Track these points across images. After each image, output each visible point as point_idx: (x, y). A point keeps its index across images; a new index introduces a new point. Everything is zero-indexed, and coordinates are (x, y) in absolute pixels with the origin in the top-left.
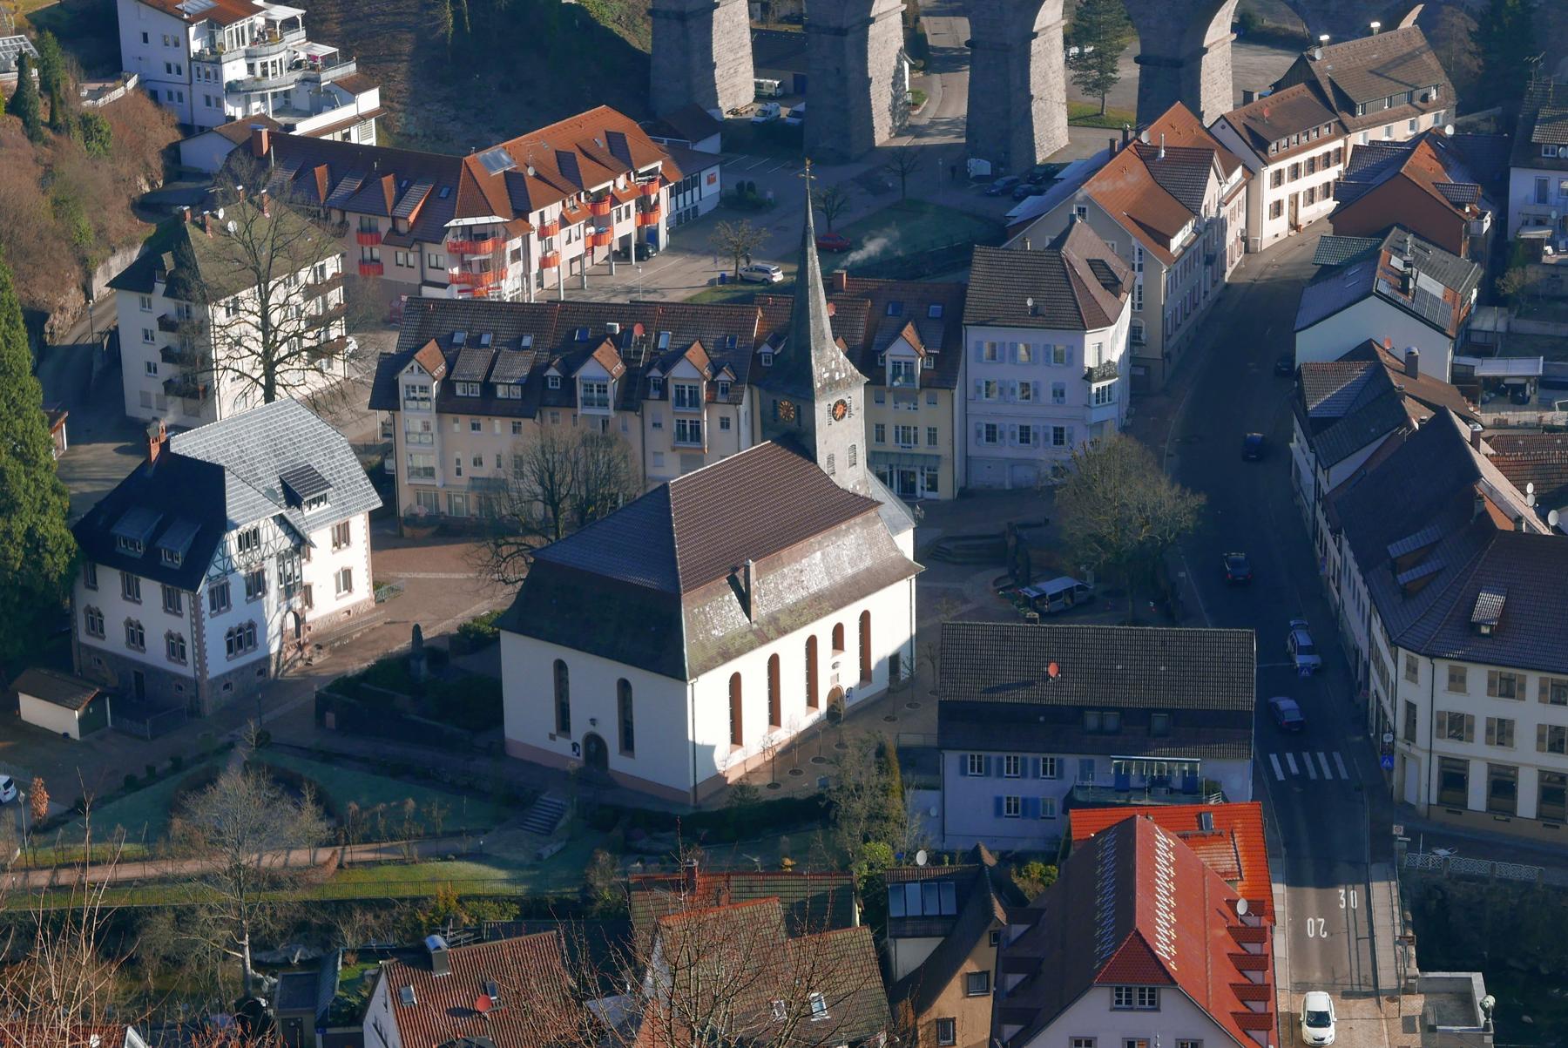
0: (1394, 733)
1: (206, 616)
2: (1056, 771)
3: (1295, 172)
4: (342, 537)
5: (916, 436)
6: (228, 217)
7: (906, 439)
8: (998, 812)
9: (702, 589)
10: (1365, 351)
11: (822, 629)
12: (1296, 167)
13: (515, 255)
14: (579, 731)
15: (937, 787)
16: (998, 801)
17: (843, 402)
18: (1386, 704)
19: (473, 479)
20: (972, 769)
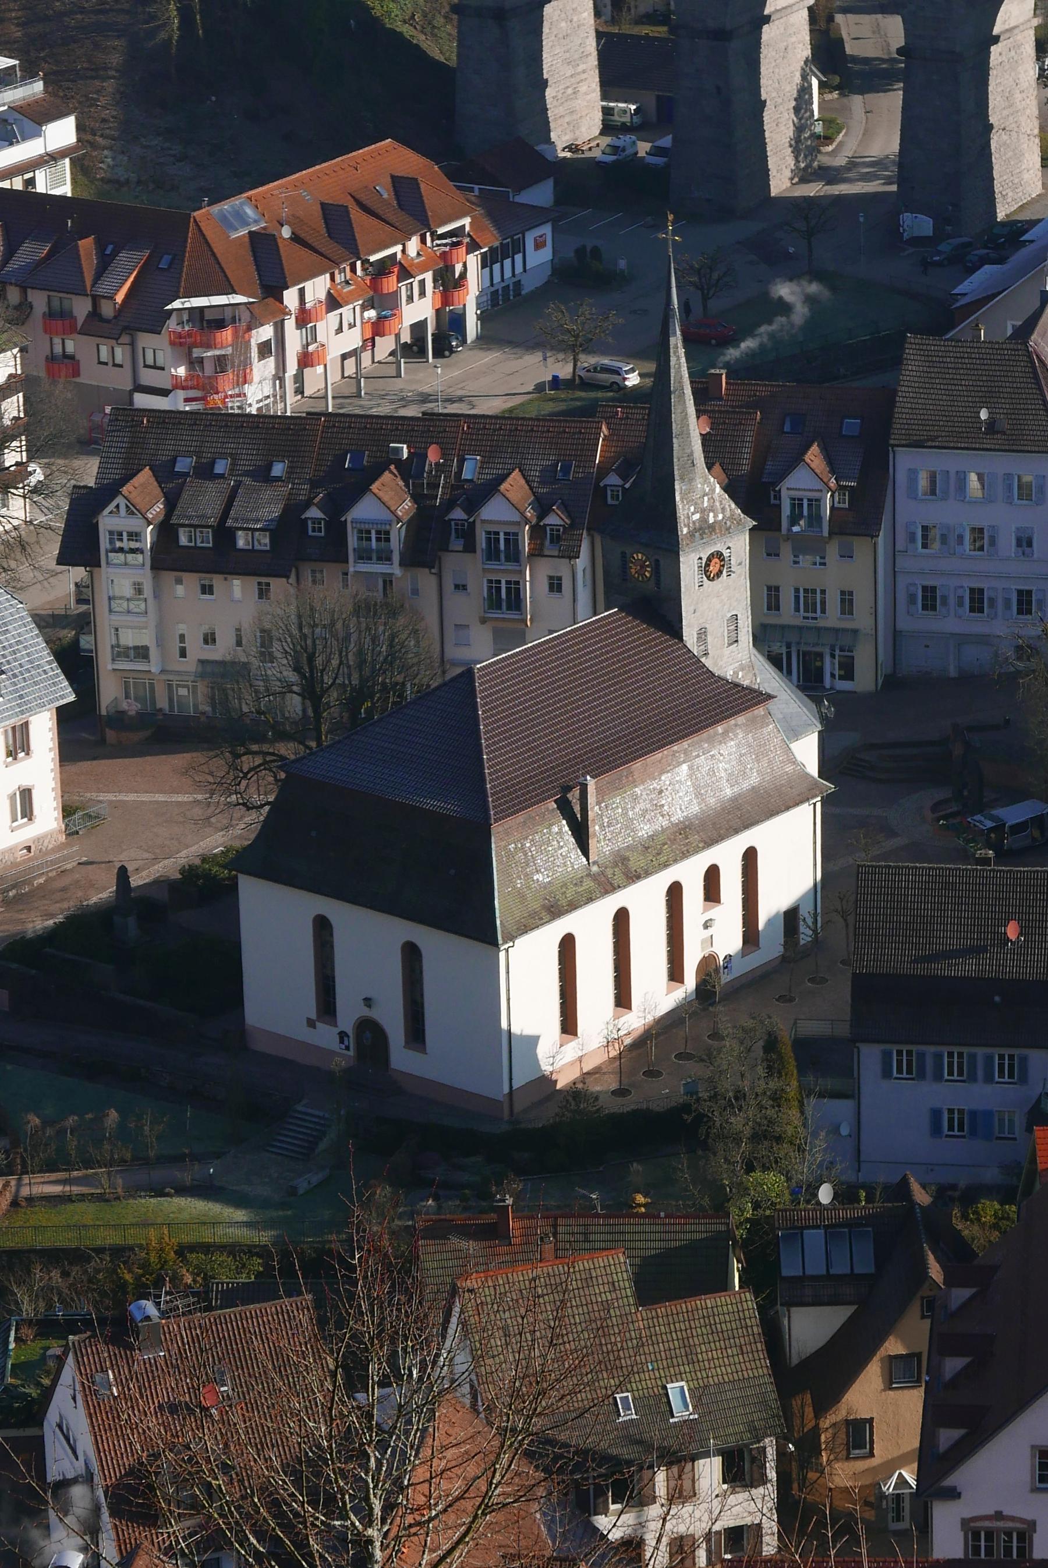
5: (823, 603)
7: (810, 607)
8: (936, 1130)
9: (521, 817)
13: (265, 349)
14: (349, 1012)
15: (851, 1093)
16: (936, 1114)
17: (719, 555)
19: (202, 662)
20: (900, 1070)
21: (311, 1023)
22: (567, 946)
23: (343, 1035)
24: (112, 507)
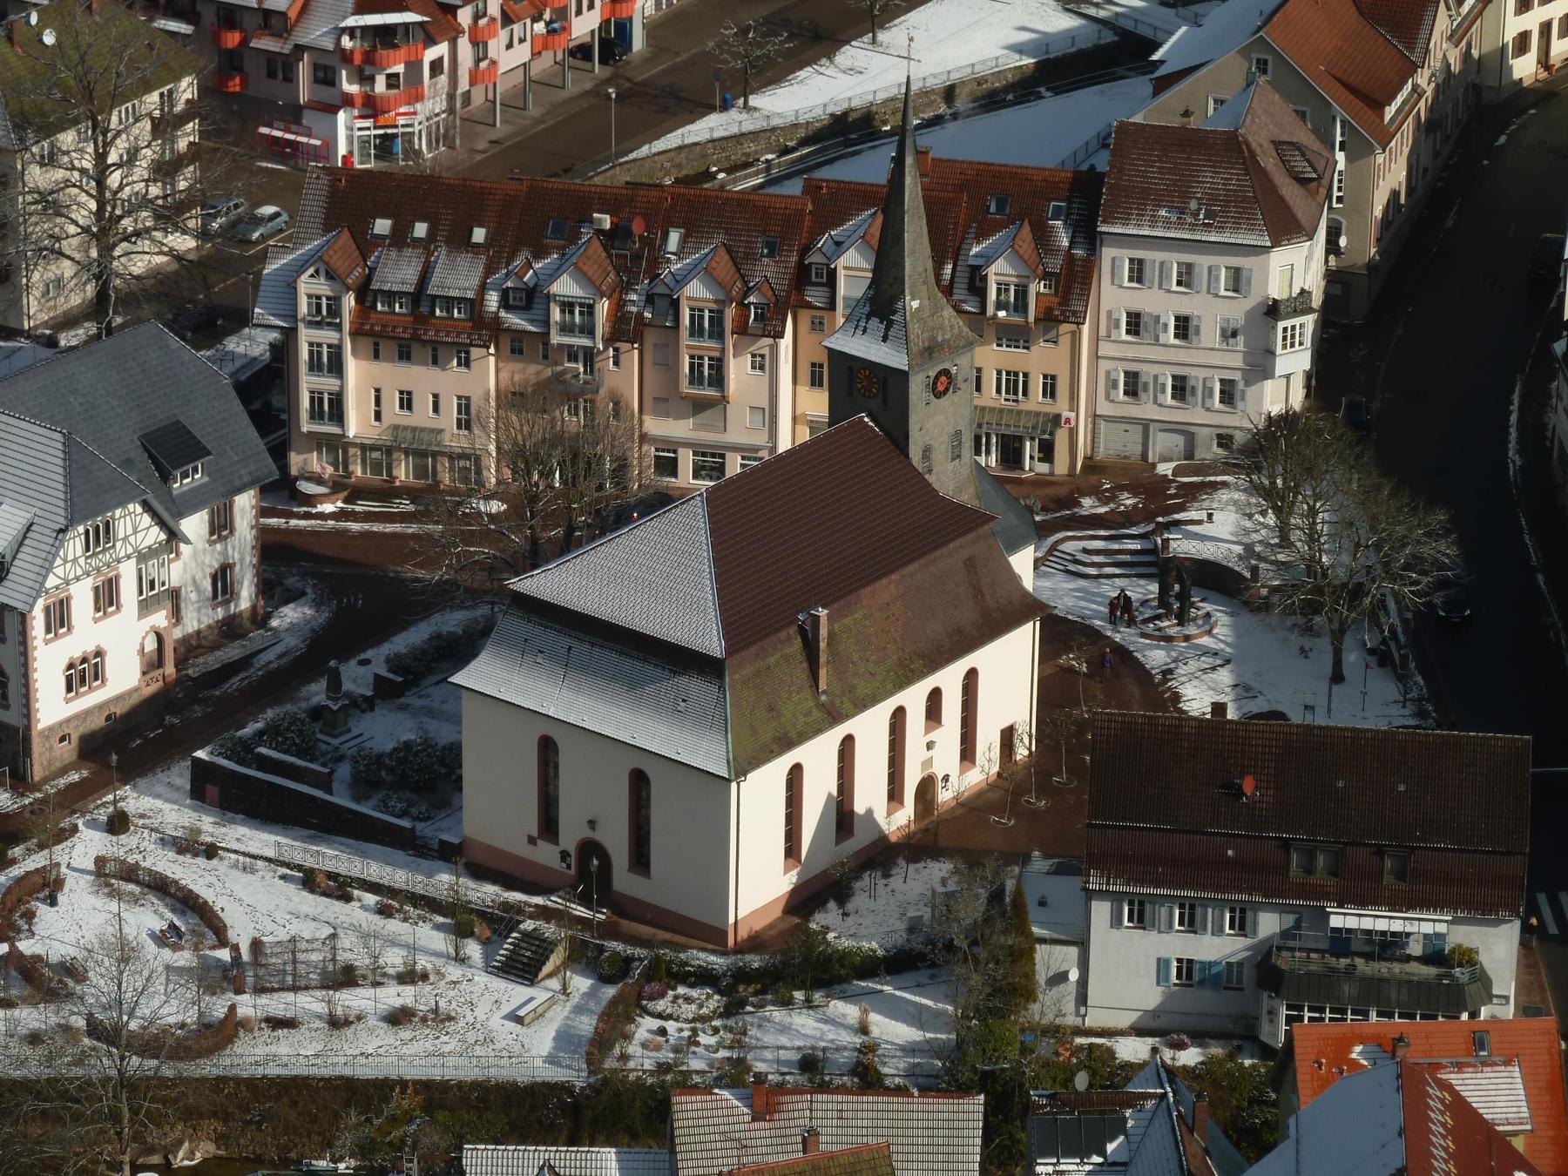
5: (1025, 384)
6: (42, 24)
7: (1012, 388)
9: (753, 649)
11: (913, 698)
13: (436, 66)
14: (571, 834)
17: (946, 372)
19: (396, 427)
20: (1130, 919)
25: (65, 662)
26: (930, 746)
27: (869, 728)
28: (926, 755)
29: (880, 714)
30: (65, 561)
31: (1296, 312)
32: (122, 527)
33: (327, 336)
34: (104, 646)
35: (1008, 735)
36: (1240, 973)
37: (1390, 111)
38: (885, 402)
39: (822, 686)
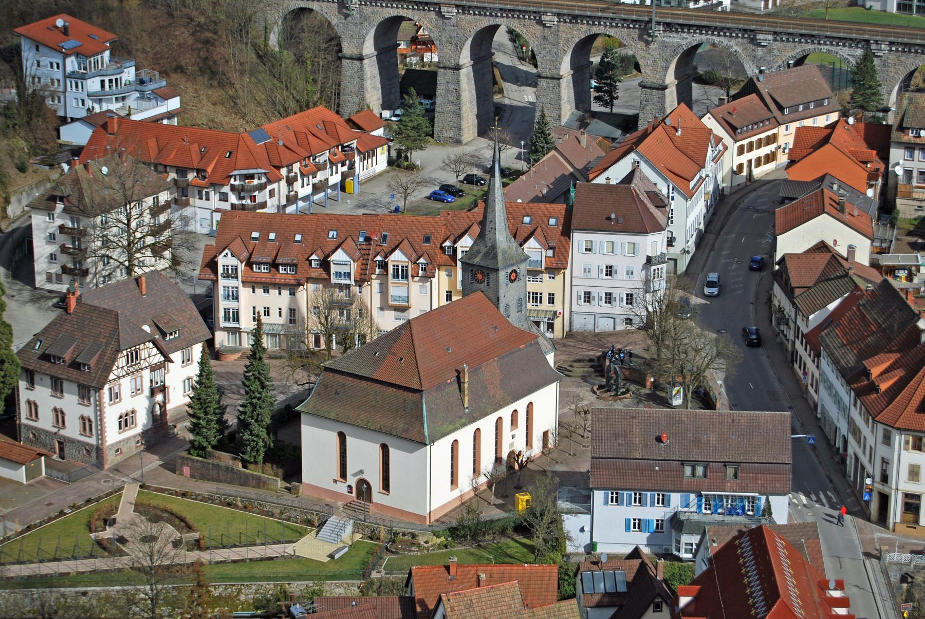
0: (873, 478)
1: (106, 405)
2: (665, 502)
3: (751, 147)
4: (187, 360)
5: (541, 298)
8: (628, 528)
10: (822, 247)
11: (505, 413)
12: (751, 144)
15: (589, 511)
16: (628, 521)
17: (515, 271)
18: (864, 460)
21: (335, 481)
22: (455, 445)
23: (350, 487)
24: (224, 253)
25: (118, 416)
26: (513, 437)
27: (487, 425)
28: (511, 441)
29: (491, 419)
30: (118, 368)
31: (660, 263)
32: (144, 354)
33: (232, 283)
34: (136, 409)
35: (545, 434)
36: (662, 525)
37: (692, 184)
38: (488, 284)
39: (466, 405)
